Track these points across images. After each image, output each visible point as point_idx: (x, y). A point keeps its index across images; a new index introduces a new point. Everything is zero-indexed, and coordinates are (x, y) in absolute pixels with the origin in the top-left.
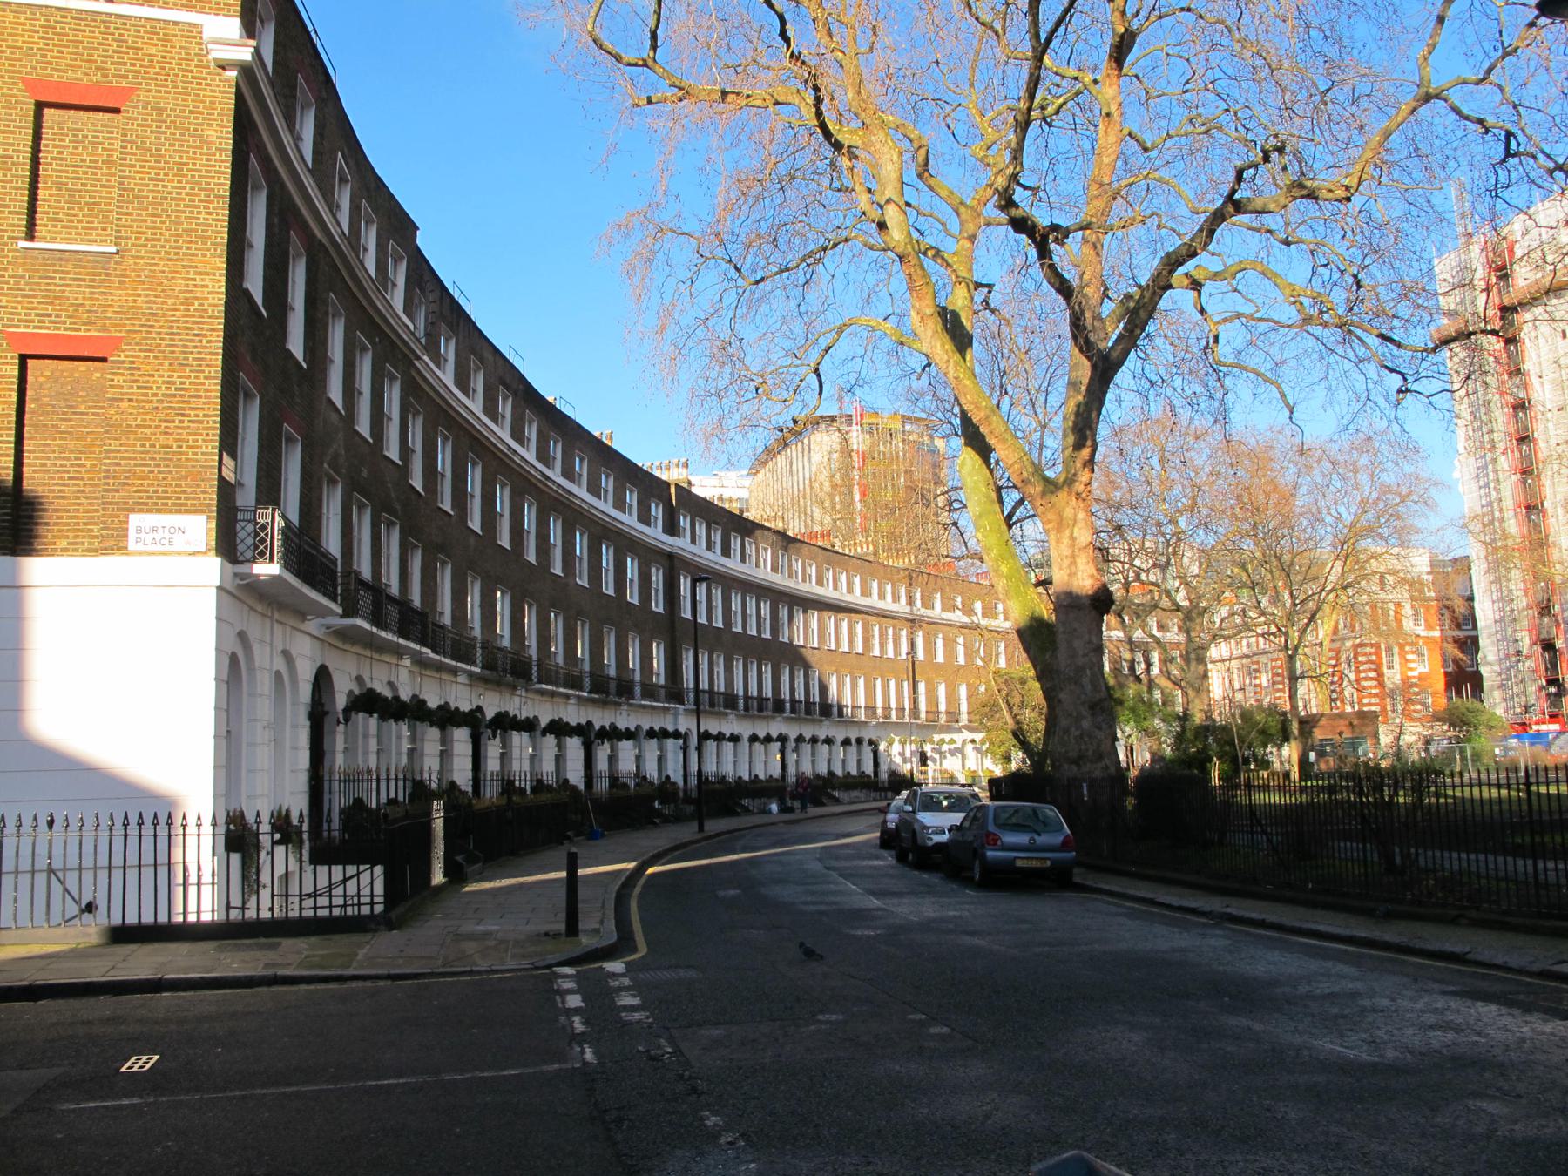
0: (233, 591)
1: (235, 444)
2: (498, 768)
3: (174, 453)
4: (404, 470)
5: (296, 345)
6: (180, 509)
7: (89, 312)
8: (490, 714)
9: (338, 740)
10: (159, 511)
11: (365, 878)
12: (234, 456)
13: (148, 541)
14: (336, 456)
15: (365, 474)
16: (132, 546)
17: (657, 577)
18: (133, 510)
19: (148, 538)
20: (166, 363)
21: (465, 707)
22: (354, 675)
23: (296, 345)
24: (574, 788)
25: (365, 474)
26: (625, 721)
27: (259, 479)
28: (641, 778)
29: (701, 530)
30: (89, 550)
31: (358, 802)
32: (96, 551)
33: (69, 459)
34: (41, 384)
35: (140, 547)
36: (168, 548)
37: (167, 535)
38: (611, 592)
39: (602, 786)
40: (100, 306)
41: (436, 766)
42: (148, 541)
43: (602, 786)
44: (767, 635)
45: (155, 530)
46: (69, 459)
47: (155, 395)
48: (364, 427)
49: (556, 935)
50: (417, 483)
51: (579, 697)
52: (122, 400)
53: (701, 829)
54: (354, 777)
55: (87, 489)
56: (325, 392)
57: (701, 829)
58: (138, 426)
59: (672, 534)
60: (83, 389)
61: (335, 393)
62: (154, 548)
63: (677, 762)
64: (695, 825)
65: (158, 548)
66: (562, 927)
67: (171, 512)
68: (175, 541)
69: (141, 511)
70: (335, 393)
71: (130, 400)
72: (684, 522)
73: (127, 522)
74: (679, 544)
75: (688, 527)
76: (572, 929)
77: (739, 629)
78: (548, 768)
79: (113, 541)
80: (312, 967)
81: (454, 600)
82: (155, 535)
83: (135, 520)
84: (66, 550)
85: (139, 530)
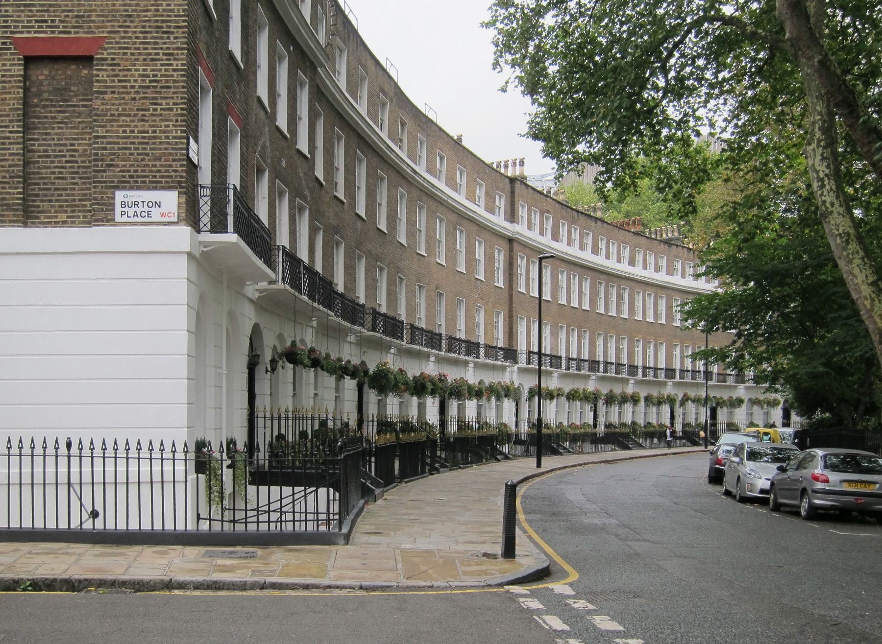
0: (198, 255)
1: (197, 131)
2: (376, 412)
3: (150, 138)
4: (309, 162)
5: (235, 45)
6: (155, 186)
7: (77, 16)
8: (372, 368)
9: (263, 386)
10: (139, 188)
11: (311, 498)
12: (196, 141)
13: (131, 214)
14: (264, 147)
15: (284, 164)
16: (118, 218)
17: (500, 259)
18: (117, 188)
19: (131, 212)
20: (141, 58)
21: (355, 361)
22: (277, 333)
23: (235, 45)
24: (431, 427)
25: (284, 164)
26: (472, 377)
27: (213, 162)
28: (483, 425)
29: (536, 219)
30: (84, 222)
31: (281, 437)
32: (89, 223)
33: (65, 145)
34: (41, 81)
35: (125, 219)
36: (147, 219)
37: (146, 209)
38: (463, 269)
39: (453, 428)
40: (86, 11)
41: (694, 416)
42: (131, 214)
43: (453, 428)
44: (586, 307)
45: (136, 204)
46: (65, 145)
47: (133, 87)
48: (282, 122)
49: (494, 556)
50: (320, 173)
51: (437, 356)
52: (106, 93)
53: (539, 465)
54: (276, 418)
55: (81, 170)
56: (255, 91)
57: (539, 465)
58: (119, 115)
59: (512, 222)
60: (74, 85)
61: (262, 91)
62: (136, 219)
63: (510, 410)
64: (534, 461)
65: (140, 219)
66: (498, 549)
67: (148, 189)
68: (153, 214)
69: (124, 188)
70: (262, 91)
71: (113, 92)
72: (522, 212)
73: (114, 198)
74: (519, 229)
75: (525, 216)
76: (509, 551)
77: (564, 302)
78: (413, 414)
79: (101, 214)
80: (288, 575)
81: (346, 273)
82: (136, 209)
83: (120, 196)
84: (64, 222)
85: (123, 204)
